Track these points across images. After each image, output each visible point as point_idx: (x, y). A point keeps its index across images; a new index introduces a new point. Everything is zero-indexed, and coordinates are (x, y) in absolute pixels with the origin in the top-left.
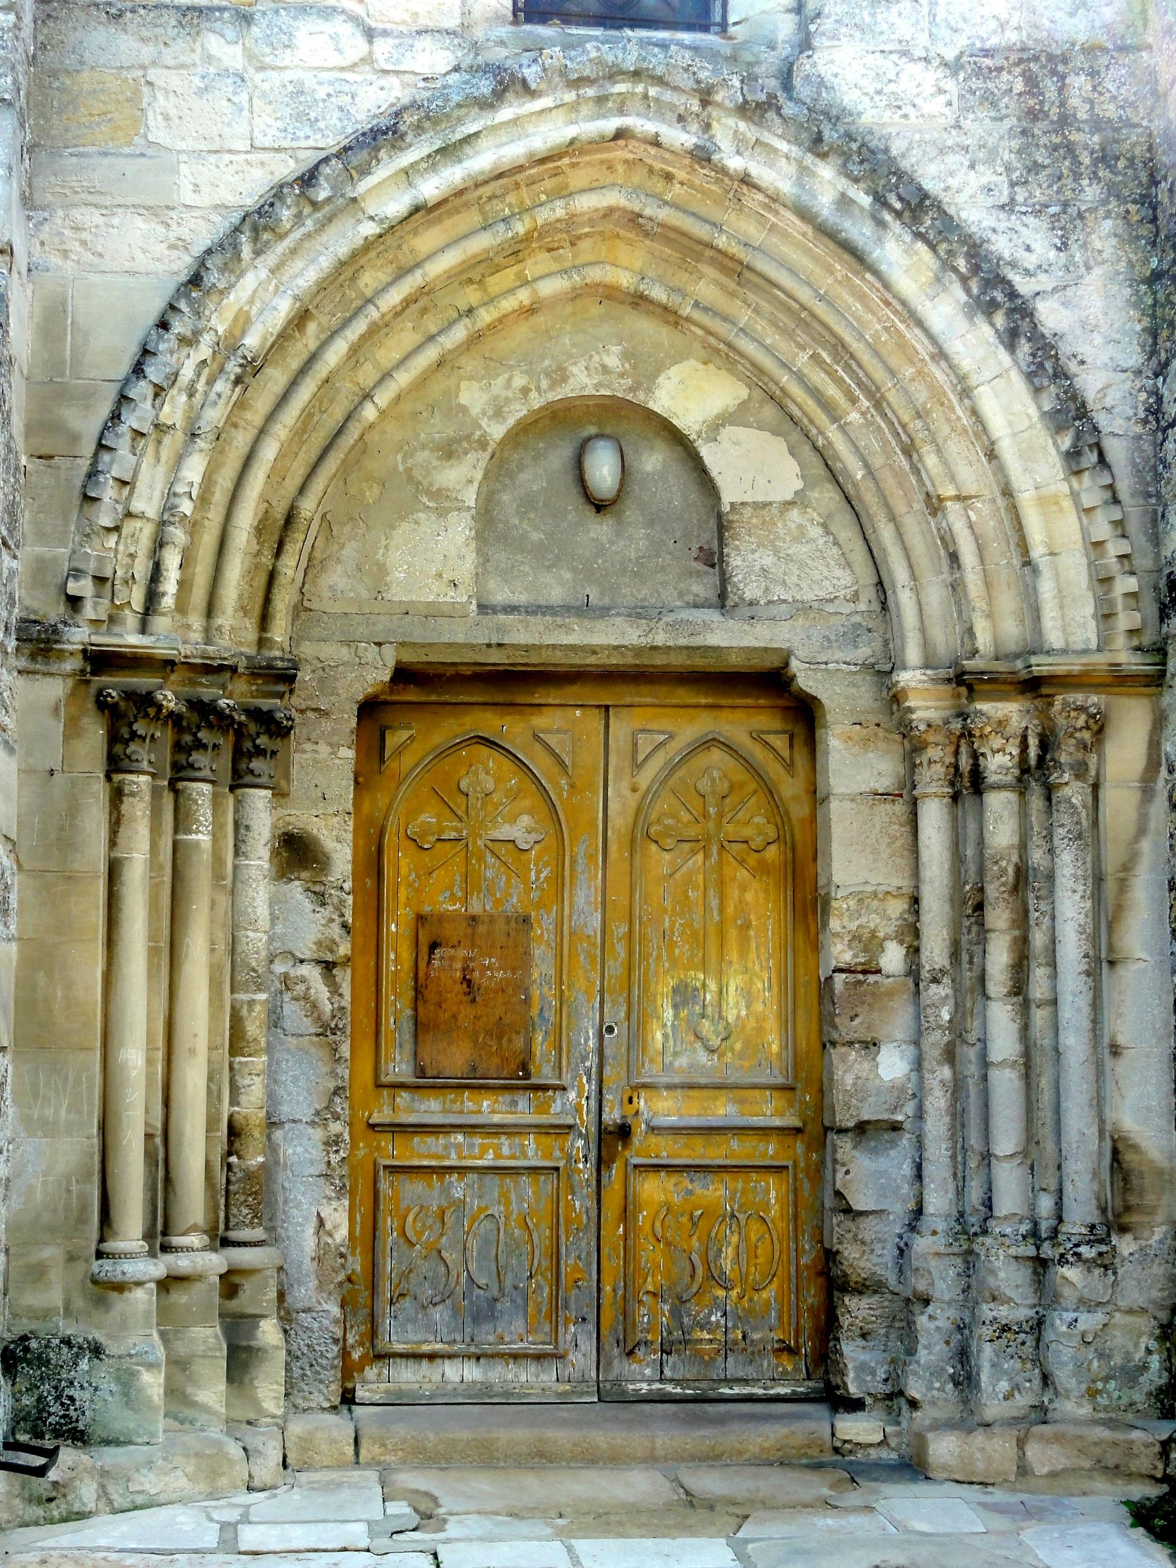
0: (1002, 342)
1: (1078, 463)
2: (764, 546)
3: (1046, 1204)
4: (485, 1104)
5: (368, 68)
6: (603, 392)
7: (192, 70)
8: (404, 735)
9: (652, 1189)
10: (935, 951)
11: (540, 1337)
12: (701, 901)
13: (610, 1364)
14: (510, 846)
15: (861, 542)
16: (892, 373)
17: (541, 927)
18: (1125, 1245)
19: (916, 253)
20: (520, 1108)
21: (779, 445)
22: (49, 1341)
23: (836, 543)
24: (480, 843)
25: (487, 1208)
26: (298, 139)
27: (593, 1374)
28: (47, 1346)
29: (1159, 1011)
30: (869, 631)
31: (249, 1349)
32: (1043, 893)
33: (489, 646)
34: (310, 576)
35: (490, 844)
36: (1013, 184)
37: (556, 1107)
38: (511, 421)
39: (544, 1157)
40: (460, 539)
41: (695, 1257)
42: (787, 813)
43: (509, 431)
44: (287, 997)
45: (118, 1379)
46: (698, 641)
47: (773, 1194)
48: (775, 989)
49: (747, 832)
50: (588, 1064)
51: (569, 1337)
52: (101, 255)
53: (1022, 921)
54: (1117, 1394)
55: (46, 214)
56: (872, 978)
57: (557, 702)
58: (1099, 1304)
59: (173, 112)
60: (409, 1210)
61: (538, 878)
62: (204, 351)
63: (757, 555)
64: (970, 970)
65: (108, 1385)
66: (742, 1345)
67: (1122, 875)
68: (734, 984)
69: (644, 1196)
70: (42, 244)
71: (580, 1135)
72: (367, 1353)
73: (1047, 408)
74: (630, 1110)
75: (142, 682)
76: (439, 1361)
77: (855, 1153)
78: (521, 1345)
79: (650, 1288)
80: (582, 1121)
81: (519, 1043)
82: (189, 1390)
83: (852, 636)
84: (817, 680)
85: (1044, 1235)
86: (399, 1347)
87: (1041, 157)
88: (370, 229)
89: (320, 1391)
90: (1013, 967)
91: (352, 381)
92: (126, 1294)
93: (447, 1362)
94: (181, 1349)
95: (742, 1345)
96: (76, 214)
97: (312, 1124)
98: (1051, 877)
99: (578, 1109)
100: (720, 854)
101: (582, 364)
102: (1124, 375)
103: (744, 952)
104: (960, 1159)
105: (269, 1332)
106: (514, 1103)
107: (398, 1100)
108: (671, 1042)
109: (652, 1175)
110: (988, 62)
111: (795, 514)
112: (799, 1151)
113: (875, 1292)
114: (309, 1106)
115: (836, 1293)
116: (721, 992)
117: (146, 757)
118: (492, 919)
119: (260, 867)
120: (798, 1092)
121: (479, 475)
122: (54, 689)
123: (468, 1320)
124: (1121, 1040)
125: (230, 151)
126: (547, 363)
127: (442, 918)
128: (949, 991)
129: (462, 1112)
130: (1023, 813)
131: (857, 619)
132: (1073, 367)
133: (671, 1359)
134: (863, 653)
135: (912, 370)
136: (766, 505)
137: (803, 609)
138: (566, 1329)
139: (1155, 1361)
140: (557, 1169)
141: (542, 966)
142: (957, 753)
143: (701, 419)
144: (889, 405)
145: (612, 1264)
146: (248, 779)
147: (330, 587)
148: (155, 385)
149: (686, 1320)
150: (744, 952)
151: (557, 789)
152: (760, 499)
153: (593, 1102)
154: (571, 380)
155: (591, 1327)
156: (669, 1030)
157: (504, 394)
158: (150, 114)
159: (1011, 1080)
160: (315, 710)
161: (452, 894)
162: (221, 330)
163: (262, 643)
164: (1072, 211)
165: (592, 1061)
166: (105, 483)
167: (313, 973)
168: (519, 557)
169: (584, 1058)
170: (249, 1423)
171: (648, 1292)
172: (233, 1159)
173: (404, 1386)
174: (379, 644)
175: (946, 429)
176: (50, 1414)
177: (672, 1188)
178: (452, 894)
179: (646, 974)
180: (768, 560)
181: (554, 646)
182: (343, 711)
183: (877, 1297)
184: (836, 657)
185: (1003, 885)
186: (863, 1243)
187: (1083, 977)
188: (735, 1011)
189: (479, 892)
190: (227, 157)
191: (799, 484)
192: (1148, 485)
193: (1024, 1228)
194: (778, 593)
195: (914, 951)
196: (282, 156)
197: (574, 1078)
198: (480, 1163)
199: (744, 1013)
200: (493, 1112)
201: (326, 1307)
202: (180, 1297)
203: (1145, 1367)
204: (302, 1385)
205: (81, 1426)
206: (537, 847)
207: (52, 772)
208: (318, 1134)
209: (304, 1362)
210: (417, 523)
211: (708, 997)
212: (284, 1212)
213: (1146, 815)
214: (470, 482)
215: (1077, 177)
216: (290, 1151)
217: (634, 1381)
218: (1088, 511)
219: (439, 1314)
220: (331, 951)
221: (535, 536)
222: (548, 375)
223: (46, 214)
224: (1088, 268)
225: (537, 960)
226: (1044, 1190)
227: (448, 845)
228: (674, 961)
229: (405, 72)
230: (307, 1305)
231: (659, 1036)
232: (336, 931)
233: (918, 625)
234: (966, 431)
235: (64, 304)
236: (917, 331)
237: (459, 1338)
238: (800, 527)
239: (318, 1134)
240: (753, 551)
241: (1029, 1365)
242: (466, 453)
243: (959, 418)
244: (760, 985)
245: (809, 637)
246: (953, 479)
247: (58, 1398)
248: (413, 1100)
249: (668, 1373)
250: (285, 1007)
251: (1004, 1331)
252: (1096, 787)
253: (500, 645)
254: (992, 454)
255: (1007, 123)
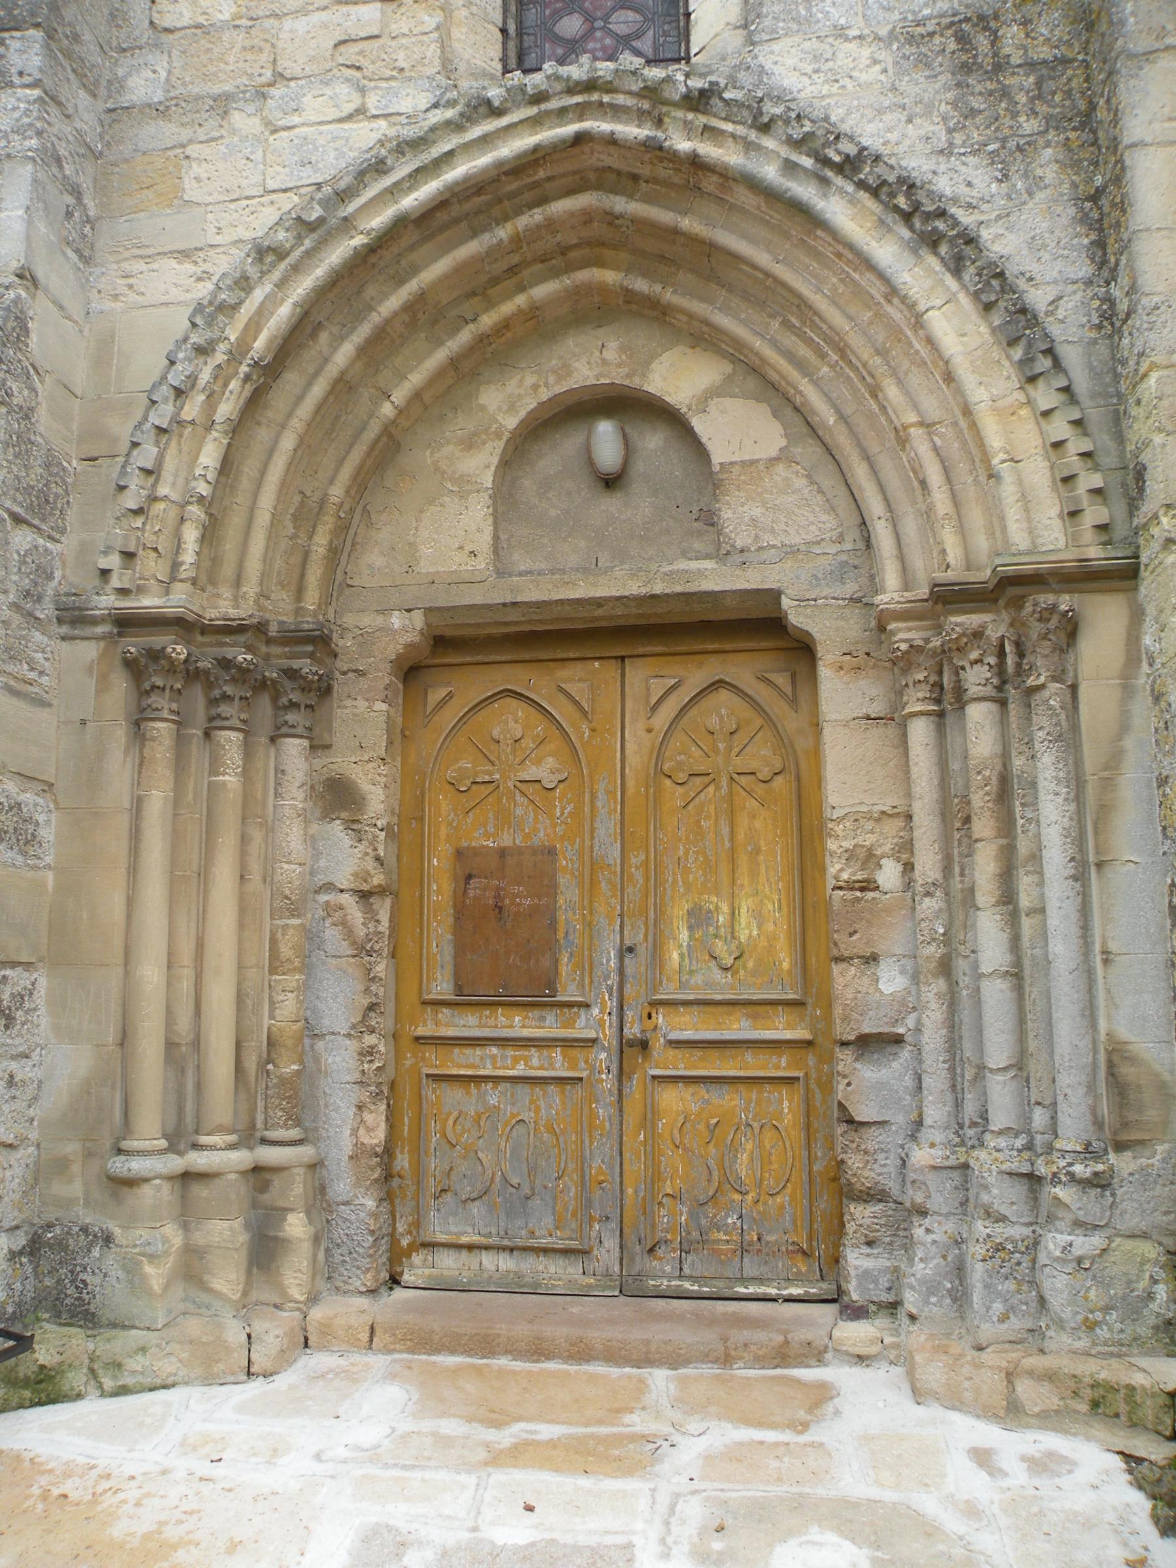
0: (948, 269)
1: (1031, 369)
2: (753, 499)
3: (1039, 1118)
4: (517, 1019)
5: (361, 117)
6: (603, 381)
7: (220, 141)
8: (442, 692)
9: (672, 1099)
10: (928, 865)
11: (568, 1233)
12: (712, 829)
13: (632, 1260)
14: (537, 786)
15: (844, 488)
16: (850, 318)
17: (565, 858)
18: (1123, 1163)
19: (859, 201)
20: (548, 1023)
21: (763, 410)
22: (70, 1229)
23: (820, 491)
24: (510, 784)
25: (518, 1114)
26: (302, 178)
27: (617, 1269)
28: (68, 1233)
29: (1155, 913)
30: (855, 567)
31: (276, 1239)
32: (1029, 799)
33: (504, 605)
34: (352, 558)
35: (519, 784)
36: (950, 131)
37: (581, 1022)
38: (523, 413)
39: (570, 1068)
40: (479, 515)
41: (712, 1163)
42: (792, 745)
43: (522, 422)
44: (328, 923)
45: (124, 1268)
46: (693, 587)
47: (786, 1104)
48: (785, 910)
49: (754, 765)
50: (609, 982)
51: (593, 1234)
52: (143, 294)
53: (1007, 827)
54: (1118, 1325)
55: (104, 270)
56: (870, 895)
57: (577, 655)
58: (1096, 1227)
59: (204, 176)
60: (450, 1114)
61: (562, 814)
62: (220, 357)
63: (746, 508)
64: (962, 882)
65: (116, 1272)
66: (757, 1246)
67: (1106, 774)
68: (745, 906)
69: (663, 1105)
70: (99, 292)
71: (603, 1048)
72: (414, 1241)
73: (996, 323)
74: (649, 1024)
75: (157, 640)
76: (476, 1251)
77: (858, 1065)
78: (550, 1240)
79: (669, 1191)
80: (605, 1035)
81: (546, 962)
82: (206, 1277)
83: (841, 573)
84: (807, 616)
85: (1039, 1151)
86: (442, 1238)
87: (977, 103)
88: (359, 241)
89: (358, 1276)
90: (1001, 875)
91: (374, 387)
92: (135, 1189)
93: (484, 1252)
94: (199, 1238)
95: (757, 1246)
96: (125, 265)
97: (349, 1036)
98: (1033, 785)
99: (601, 1023)
100: (730, 787)
101: (584, 359)
102: (1075, 287)
103: (754, 874)
104: (958, 1071)
105: (296, 1226)
106: (543, 1019)
107: (440, 1015)
108: (687, 961)
109: (671, 1086)
110: (920, 30)
111: (780, 468)
112: (811, 1063)
113: (880, 1201)
114: (347, 1020)
115: (844, 1200)
116: (733, 913)
117: (166, 706)
118: (519, 851)
119: (294, 807)
120: (809, 1007)
121: (495, 460)
122: (89, 651)
123: (503, 1216)
124: (1113, 946)
125: (247, 198)
126: (554, 362)
127: (477, 852)
128: (942, 904)
129: (496, 1027)
130: (1003, 722)
131: (844, 557)
132: (1022, 284)
133: (690, 1258)
134: (850, 588)
135: (869, 314)
136: (753, 462)
137: (791, 551)
138: (591, 1227)
139: (1161, 1291)
140: (581, 1079)
141: (568, 893)
142: (940, 673)
143: (690, 395)
144: (853, 352)
145: (635, 1167)
146: (284, 730)
147: (369, 565)
148: (175, 388)
149: (703, 1222)
150: (754, 874)
151: (581, 732)
152: (747, 457)
153: (614, 1018)
154: (575, 374)
155: (614, 1225)
156: (685, 950)
157: (517, 392)
158: (186, 180)
159: (1002, 991)
160: (354, 671)
161: (486, 831)
162: (233, 338)
163: (299, 611)
164: (1011, 144)
165: (614, 980)
166: (132, 473)
167: (347, 900)
168: (539, 532)
169: (607, 977)
170: (276, 1306)
171: (667, 1195)
172: (270, 1067)
173: (446, 1273)
174: (409, 611)
175: (906, 364)
176: (66, 1295)
177: (689, 1098)
178: (486, 831)
179: (662, 899)
180: (757, 512)
181: (561, 602)
182: (380, 670)
183: (880, 1206)
184: (824, 594)
185: (987, 794)
186: (866, 1152)
187: (1071, 882)
188: (747, 932)
189: (509, 828)
190: (244, 203)
191: (783, 442)
192: (1107, 386)
193: (1019, 1142)
194: (767, 539)
195: (909, 867)
196: (289, 194)
197: (597, 995)
198: (511, 1073)
199: (755, 933)
200: (523, 1027)
201: (362, 1201)
202: (200, 1191)
203: (1150, 1296)
204: (342, 1269)
205: (92, 1308)
206: (561, 786)
207: (83, 722)
208: (353, 1045)
209: (344, 1250)
210: (442, 505)
211: (721, 919)
212: (325, 1114)
213: (1128, 711)
214: (488, 467)
215: (1014, 115)
216: (330, 1060)
217: (654, 1277)
218: (1046, 414)
219: (476, 1209)
220: (365, 881)
221: (553, 513)
222: (554, 372)
223: (104, 270)
224: (1030, 194)
225: (562, 888)
226: (1039, 1104)
227: (483, 786)
228: (688, 887)
229: (391, 114)
230: (346, 1199)
231: (675, 955)
232: (370, 865)
233: (895, 552)
234: (925, 363)
235: (112, 337)
236: (868, 275)
237: (494, 1231)
238: (786, 479)
239: (353, 1045)
240: (743, 504)
241: (1025, 1287)
242: (484, 443)
243: (917, 352)
244: (770, 907)
245: (797, 577)
246: (916, 407)
247: (73, 1281)
248: (453, 1015)
249: (687, 1271)
250: (327, 931)
251: (998, 1250)
252: (1074, 688)
253: (514, 604)
254: (949, 377)
255: (942, 79)
